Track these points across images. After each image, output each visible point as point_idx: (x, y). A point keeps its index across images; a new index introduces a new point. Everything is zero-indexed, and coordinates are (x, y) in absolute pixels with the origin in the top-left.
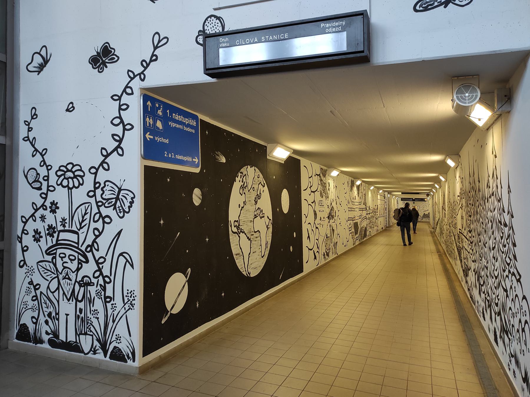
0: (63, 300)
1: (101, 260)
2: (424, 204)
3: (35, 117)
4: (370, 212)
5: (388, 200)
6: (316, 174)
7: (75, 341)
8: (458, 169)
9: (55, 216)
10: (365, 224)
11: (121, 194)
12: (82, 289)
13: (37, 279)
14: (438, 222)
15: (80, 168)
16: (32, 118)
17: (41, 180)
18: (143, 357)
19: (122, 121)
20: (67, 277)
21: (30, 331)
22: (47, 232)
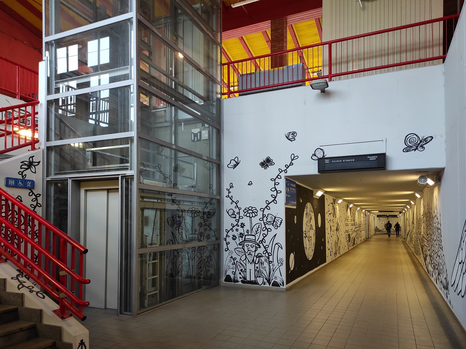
0: (248, 264)
1: (267, 247)
2: (396, 220)
3: (232, 187)
4: (357, 227)
5: (368, 217)
6: (331, 203)
7: (254, 280)
8: (422, 199)
9: (243, 229)
10: (353, 235)
11: (276, 219)
12: (258, 259)
13: (234, 255)
14: (408, 233)
15: (255, 209)
16: (231, 187)
17: (236, 214)
18: (286, 285)
19: (276, 189)
20: (250, 254)
21: (232, 278)
22: (239, 236)
